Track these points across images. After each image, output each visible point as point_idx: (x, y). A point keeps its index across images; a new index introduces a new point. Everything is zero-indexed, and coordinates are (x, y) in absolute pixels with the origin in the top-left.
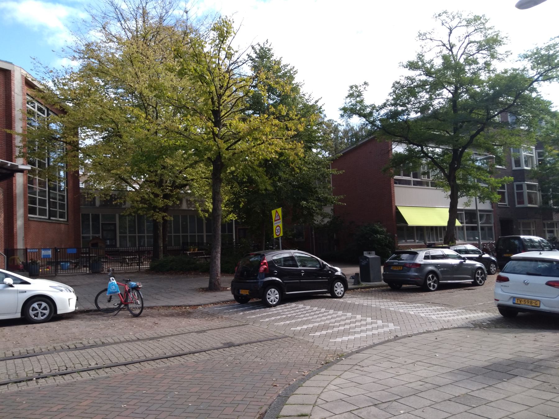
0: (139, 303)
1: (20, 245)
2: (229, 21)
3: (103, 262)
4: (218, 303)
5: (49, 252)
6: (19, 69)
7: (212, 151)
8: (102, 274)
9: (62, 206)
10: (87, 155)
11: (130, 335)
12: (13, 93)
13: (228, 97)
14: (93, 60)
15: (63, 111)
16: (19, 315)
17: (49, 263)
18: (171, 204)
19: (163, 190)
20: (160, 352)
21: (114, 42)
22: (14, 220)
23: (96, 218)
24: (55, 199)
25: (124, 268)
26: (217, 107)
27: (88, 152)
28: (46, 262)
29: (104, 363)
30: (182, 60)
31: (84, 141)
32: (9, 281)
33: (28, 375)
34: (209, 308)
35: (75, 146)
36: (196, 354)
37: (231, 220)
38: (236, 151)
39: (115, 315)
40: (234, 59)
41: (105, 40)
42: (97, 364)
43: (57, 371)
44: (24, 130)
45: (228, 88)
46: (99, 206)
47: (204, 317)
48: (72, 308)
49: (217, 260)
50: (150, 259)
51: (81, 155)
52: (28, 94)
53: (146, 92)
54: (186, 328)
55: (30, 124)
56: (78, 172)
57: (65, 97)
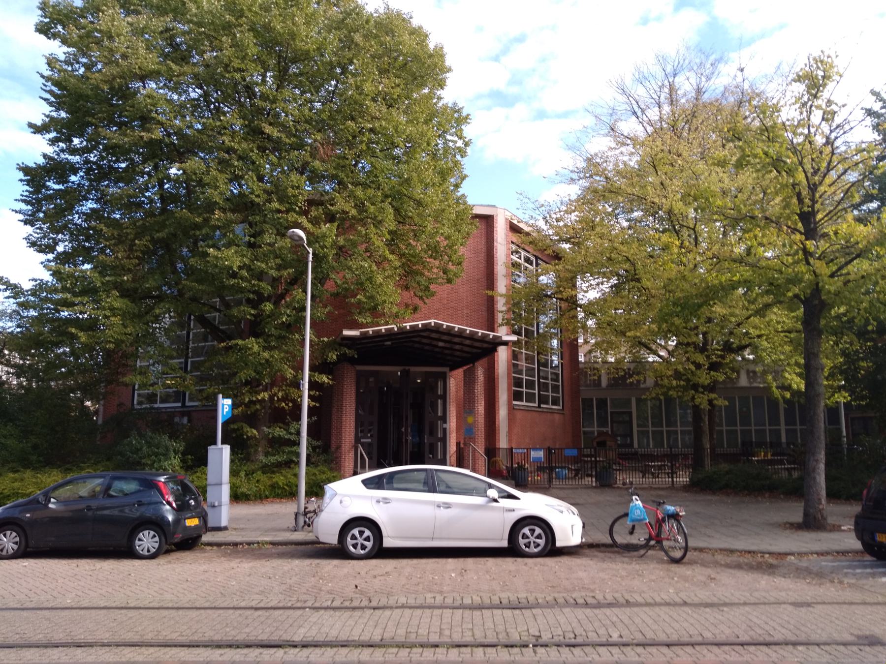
0: (680, 541)
1: (503, 443)
2: (829, 57)
3: (616, 470)
4: (827, 553)
5: (541, 454)
6: (503, 211)
7: (802, 282)
8: (614, 488)
9: (555, 389)
10: (590, 314)
11: (670, 593)
12: (495, 243)
13: (830, 186)
14: (598, 178)
15: (557, 257)
16: (505, 544)
17: (540, 469)
18: (721, 378)
19: (708, 357)
20: (727, 631)
21: (628, 145)
22: (497, 409)
23: (602, 403)
24: (547, 378)
25: (648, 481)
26: (809, 207)
27: (590, 309)
28: (536, 467)
29: (632, 637)
30: (741, 143)
31: (586, 295)
32: (493, 493)
33: (522, 638)
34: (810, 560)
35: (573, 302)
36: (800, 648)
37: (837, 402)
38: (851, 277)
39: (642, 556)
40: (838, 120)
41: (613, 145)
42: (621, 636)
43: (561, 638)
44: (508, 290)
45: (828, 169)
46: (607, 386)
47: (802, 576)
48: (575, 539)
49: (819, 474)
50: (689, 468)
51: (581, 315)
52: (513, 243)
53: (679, 206)
54: (771, 594)
55: (515, 281)
56: (576, 340)
57: (561, 238)
